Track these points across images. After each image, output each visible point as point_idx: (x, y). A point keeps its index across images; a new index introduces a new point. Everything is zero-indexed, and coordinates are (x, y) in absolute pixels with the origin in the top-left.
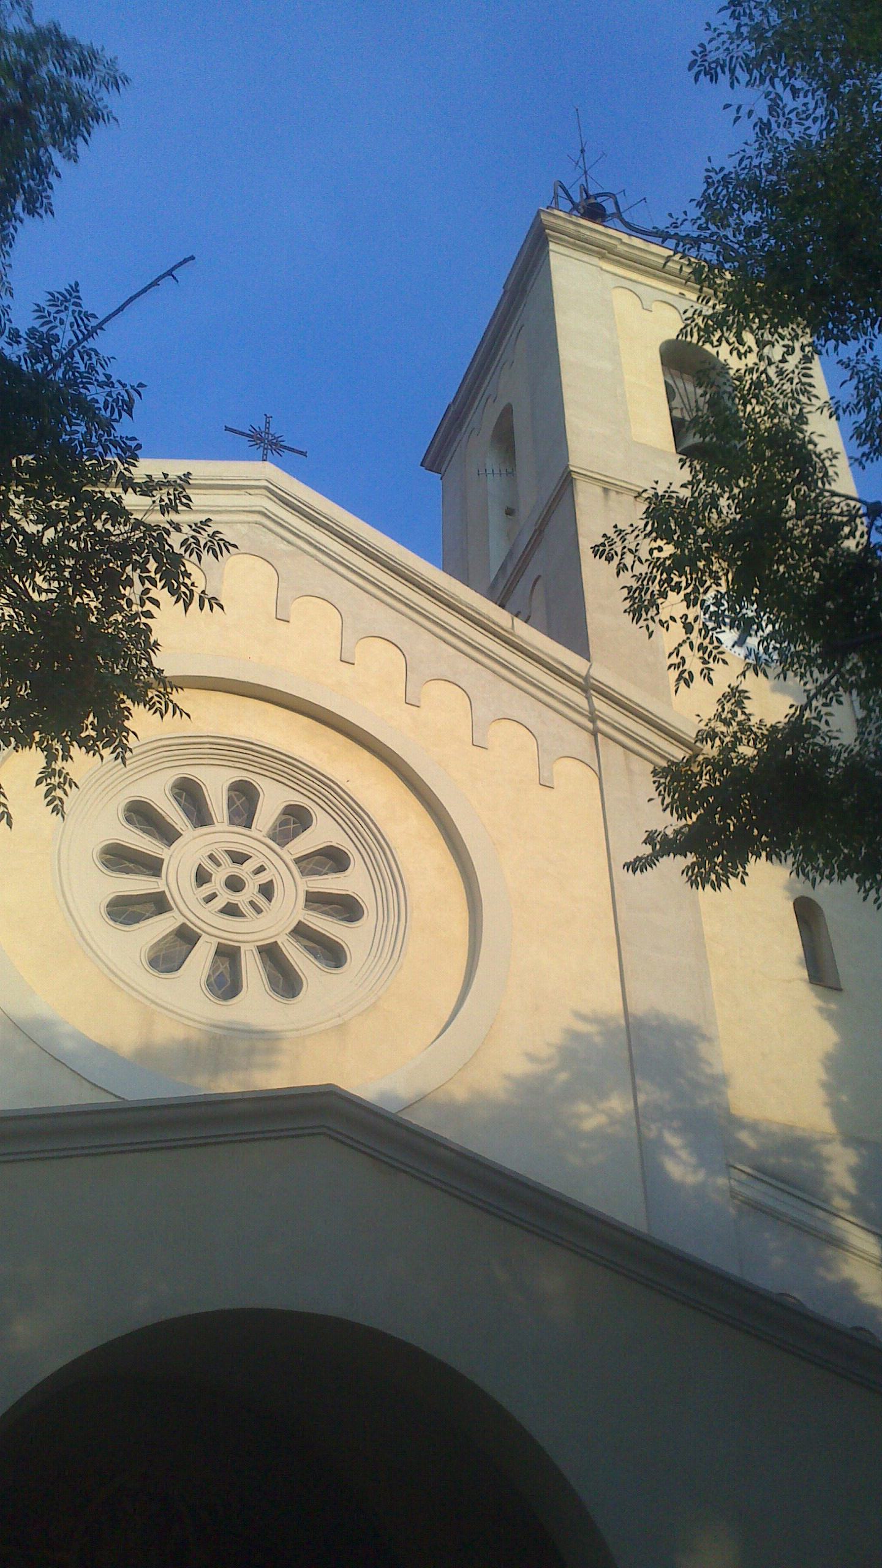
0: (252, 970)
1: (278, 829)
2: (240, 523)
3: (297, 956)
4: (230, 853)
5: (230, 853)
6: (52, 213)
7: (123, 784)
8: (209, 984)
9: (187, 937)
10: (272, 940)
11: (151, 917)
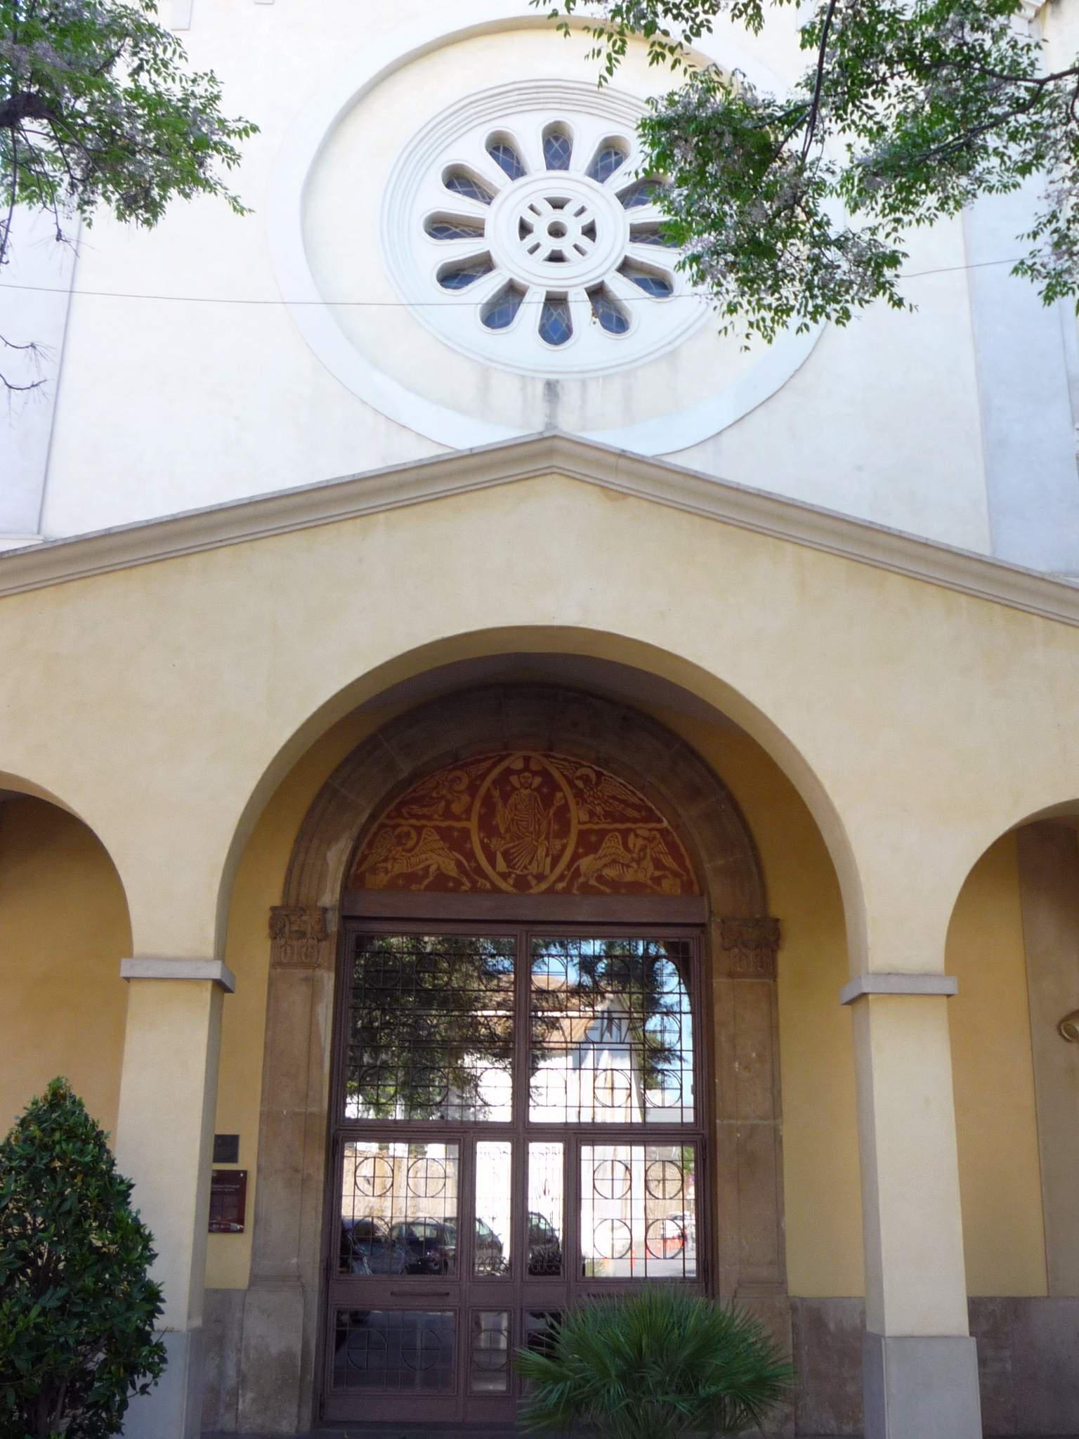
0: (581, 310)
3: (623, 289)
7: (437, 151)
8: (506, 324)
9: (513, 293)
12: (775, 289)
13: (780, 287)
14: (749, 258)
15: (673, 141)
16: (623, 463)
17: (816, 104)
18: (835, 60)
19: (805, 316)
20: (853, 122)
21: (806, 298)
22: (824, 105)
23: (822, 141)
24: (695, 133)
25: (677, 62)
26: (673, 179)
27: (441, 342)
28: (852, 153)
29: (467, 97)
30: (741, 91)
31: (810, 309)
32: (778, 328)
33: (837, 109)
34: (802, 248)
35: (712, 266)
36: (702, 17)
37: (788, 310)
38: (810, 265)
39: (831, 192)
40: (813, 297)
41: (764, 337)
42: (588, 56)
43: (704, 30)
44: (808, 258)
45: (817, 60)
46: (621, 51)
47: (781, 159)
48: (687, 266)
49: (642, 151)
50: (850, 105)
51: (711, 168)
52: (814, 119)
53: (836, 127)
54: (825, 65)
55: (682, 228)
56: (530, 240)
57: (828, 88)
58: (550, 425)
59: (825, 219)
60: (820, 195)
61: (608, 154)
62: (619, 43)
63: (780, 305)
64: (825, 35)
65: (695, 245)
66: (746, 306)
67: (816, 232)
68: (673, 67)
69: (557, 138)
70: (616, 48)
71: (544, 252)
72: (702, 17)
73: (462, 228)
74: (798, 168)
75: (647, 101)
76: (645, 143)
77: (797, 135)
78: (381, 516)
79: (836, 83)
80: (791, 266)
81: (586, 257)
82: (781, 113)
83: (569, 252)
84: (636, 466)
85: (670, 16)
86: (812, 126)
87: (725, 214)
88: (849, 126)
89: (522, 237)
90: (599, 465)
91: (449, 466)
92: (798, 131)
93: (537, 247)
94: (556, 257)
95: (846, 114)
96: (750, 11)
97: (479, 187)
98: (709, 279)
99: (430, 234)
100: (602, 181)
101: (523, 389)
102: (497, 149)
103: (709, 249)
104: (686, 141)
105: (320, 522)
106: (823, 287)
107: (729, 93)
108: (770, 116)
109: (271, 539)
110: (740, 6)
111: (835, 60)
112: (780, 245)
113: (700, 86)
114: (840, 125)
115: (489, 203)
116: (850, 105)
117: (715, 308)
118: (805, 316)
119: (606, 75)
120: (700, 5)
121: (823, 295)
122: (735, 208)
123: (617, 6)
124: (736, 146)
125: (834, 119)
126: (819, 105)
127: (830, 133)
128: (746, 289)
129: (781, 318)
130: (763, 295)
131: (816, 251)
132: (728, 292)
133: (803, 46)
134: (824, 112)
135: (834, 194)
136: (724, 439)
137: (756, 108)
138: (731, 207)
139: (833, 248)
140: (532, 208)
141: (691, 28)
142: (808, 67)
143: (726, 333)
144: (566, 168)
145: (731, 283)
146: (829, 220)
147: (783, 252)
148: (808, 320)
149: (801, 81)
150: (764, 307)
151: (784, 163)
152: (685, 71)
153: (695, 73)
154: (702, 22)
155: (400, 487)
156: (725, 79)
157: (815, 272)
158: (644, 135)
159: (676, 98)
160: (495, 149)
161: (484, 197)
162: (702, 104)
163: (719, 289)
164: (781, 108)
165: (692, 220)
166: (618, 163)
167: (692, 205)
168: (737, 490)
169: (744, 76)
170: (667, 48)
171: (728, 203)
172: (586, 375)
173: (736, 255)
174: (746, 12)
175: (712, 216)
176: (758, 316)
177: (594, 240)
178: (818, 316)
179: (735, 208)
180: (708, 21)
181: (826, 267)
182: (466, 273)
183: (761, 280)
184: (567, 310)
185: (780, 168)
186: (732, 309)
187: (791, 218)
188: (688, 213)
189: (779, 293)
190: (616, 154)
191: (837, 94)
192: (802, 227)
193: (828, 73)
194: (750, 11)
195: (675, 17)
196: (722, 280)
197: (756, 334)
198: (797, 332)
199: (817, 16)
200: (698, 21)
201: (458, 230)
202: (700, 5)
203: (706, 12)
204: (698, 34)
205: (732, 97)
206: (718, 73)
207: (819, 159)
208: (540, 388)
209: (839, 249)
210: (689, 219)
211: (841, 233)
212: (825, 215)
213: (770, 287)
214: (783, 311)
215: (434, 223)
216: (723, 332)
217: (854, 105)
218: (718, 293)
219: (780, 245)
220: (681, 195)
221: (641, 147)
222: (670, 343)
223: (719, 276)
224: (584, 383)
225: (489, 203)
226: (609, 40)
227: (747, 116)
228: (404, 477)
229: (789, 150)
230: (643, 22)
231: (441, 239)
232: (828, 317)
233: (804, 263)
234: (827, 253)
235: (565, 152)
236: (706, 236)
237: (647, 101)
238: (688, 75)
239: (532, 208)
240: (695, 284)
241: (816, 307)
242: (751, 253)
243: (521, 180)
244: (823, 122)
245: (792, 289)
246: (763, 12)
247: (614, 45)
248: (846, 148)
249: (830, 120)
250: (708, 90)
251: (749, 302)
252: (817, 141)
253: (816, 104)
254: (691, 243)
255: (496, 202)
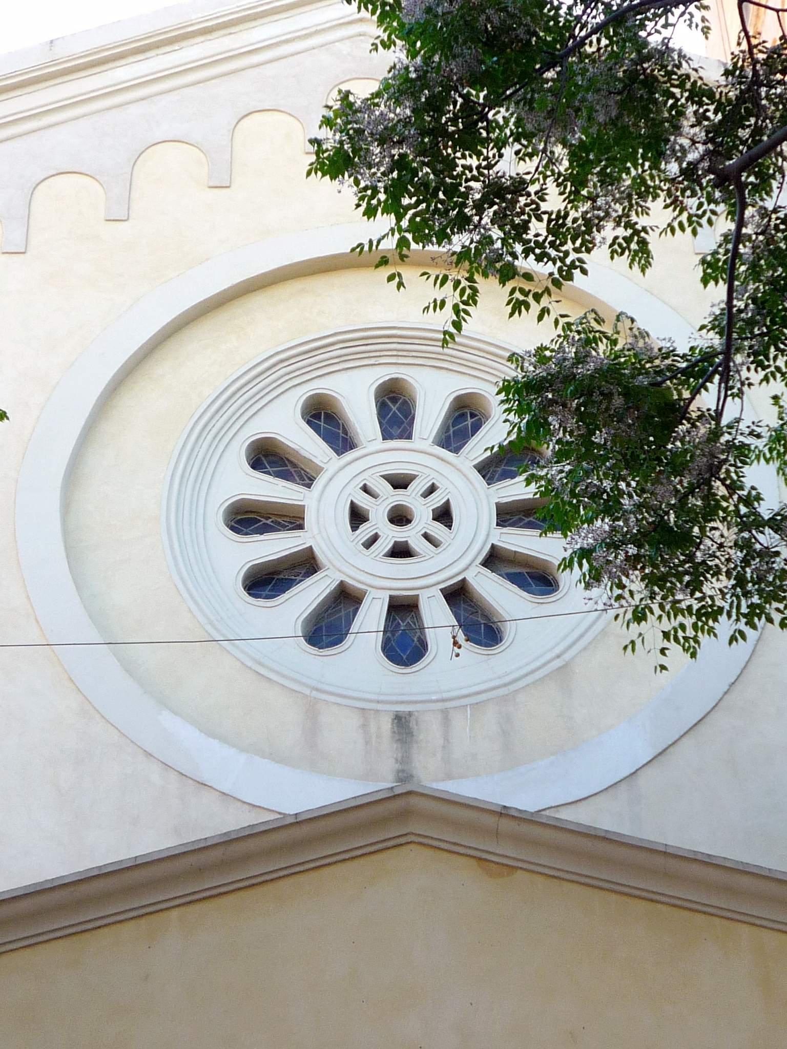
1: (452, 430)
2: (338, 41)
4: (388, 478)
5: (388, 478)
6: (715, 635)
8: (339, 641)
10: (460, 578)
11: (302, 580)
12: (695, 586)
13: (702, 583)
14: (658, 549)
15: (546, 406)
16: (505, 824)
17: (728, 351)
18: (747, 294)
19: (738, 620)
20: (778, 369)
21: (738, 597)
22: (738, 350)
23: (740, 395)
24: (574, 395)
25: (544, 312)
26: (549, 453)
27: (250, 668)
28: (781, 407)
29: (173, 475)
30: (630, 340)
31: (744, 610)
32: (704, 638)
33: (756, 354)
34: (726, 533)
35: (609, 562)
36: (573, 256)
37: (715, 613)
38: (739, 554)
39: (758, 458)
40: (747, 594)
41: (686, 650)
42: (428, 308)
43: (577, 273)
44: (736, 544)
45: (724, 297)
46: (473, 299)
47: (689, 420)
48: (576, 565)
49: (506, 421)
50: (772, 349)
51: (598, 438)
52: (728, 369)
53: (756, 376)
54: (735, 302)
55: (566, 513)
56: (365, 531)
57: (742, 330)
58: (404, 776)
59: (754, 493)
60: (745, 463)
61: (462, 416)
62: (468, 291)
63: (703, 606)
64: (733, 268)
65: (584, 538)
66: (657, 611)
67: (743, 510)
68: (540, 318)
69: (394, 400)
70: (465, 298)
71: (383, 544)
72: (573, 256)
73: (274, 518)
74: (711, 432)
75: (510, 359)
76: (509, 410)
77: (707, 390)
78: (175, 913)
79: (751, 323)
80: (713, 556)
81: (440, 549)
82: (684, 365)
83: (417, 543)
84: (524, 829)
85: (532, 257)
86: (726, 378)
87: (621, 493)
88: (773, 374)
89: (354, 528)
90: (473, 828)
91: (266, 841)
92: (708, 384)
93: (374, 539)
94: (401, 551)
95: (768, 360)
96: (634, 246)
97: (295, 465)
98: (605, 579)
99: (232, 529)
100: (456, 450)
101: (364, 726)
102: (317, 416)
103: (603, 541)
104: (564, 405)
105: (89, 926)
106: (760, 579)
107: (614, 342)
108: (669, 368)
109: (22, 950)
110: (620, 240)
111: (747, 294)
112: (696, 530)
113: (577, 337)
114: (762, 374)
115: (309, 486)
116: (772, 349)
117: (617, 617)
118: (738, 620)
119: (453, 330)
120: (569, 242)
121: (760, 592)
122: (633, 484)
123: (463, 247)
124: (629, 408)
125: (753, 367)
126: (733, 351)
127: (750, 385)
128: (656, 589)
129: (706, 623)
130: (679, 596)
131: (746, 535)
132: (631, 593)
133: (705, 281)
134: (739, 358)
135: (762, 459)
136: (642, 780)
137: (651, 360)
138: (628, 485)
139: (767, 530)
140: (365, 489)
141: (560, 270)
142: (713, 306)
143: (633, 650)
144: (409, 437)
145: (635, 583)
146: (759, 494)
147: (701, 538)
148: (742, 626)
149: (706, 322)
150: (682, 611)
151: (694, 425)
152: (556, 322)
153: (569, 324)
154: (573, 262)
155: (200, 871)
156: (608, 329)
157: (746, 562)
158: (507, 401)
159: (548, 353)
160: (314, 416)
161: (302, 479)
162: (581, 359)
163: (620, 591)
164: (684, 356)
165: (578, 501)
166: (476, 427)
167: (576, 484)
168: (665, 853)
169: (633, 320)
170: (531, 296)
171: (624, 480)
172: (448, 705)
173: (639, 546)
174: (628, 247)
175: (605, 496)
176: (675, 623)
177: (450, 527)
178: (756, 619)
179: (633, 484)
180: (580, 260)
181: (760, 554)
182: (281, 576)
183: (674, 576)
184: (418, 617)
185: (689, 432)
186: (639, 616)
187: (709, 496)
188: (573, 494)
189: (701, 591)
190: (473, 415)
191: (754, 336)
192: (724, 504)
193: (740, 311)
194: (634, 246)
195: (539, 259)
196: (624, 579)
197: (675, 649)
198: (730, 643)
199: (720, 246)
200: (568, 261)
201: (269, 522)
202: (569, 242)
203: (577, 250)
204: (570, 277)
205: (619, 347)
206: (599, 320)
207: (738, 420)
208: (386, 724)
209: (776, 532)
210: (575, 501)
211: (776, 510)
212: (753, 488)
213: (688, 585)
214: (707, 615)
215: (237, 513)
216: (630, 647)
217: (777, 349)
218: (619, 597)
219: (696, 530)
220: (561, 471)
221: (505, 416)
222: (558, 656)
223: (619, 573)
224: (445, 713)
225: (309, 486)
226: (455, 289)
227: (642, 371)
228: (203, 857)
229: (699, 409)
230: (498, 265)
231: (247, 534)
232: (770, 620)
233: (732, 552)
234: (760, 537)
235: (406, 418)
236: (598, 523)
237: (510, 359)
238: (560, 326)
239: (365, 489)
240: (588, 586)
241: (751, 606)
242: (659, 543)
243: (350, 456)
244: (738, 372)
245: (718, 585)
246: (650, 247)
247: (462, 295)
248: (772, 401)
249: (749, 369)
250: (588, 342)
251: (662, 607)
252: (732, 395)
253: (728, 351)
254: (579, 535)
255: (318, 485)
